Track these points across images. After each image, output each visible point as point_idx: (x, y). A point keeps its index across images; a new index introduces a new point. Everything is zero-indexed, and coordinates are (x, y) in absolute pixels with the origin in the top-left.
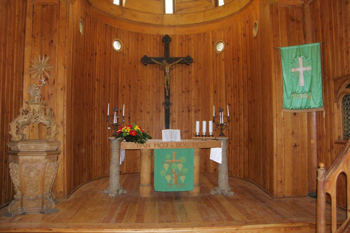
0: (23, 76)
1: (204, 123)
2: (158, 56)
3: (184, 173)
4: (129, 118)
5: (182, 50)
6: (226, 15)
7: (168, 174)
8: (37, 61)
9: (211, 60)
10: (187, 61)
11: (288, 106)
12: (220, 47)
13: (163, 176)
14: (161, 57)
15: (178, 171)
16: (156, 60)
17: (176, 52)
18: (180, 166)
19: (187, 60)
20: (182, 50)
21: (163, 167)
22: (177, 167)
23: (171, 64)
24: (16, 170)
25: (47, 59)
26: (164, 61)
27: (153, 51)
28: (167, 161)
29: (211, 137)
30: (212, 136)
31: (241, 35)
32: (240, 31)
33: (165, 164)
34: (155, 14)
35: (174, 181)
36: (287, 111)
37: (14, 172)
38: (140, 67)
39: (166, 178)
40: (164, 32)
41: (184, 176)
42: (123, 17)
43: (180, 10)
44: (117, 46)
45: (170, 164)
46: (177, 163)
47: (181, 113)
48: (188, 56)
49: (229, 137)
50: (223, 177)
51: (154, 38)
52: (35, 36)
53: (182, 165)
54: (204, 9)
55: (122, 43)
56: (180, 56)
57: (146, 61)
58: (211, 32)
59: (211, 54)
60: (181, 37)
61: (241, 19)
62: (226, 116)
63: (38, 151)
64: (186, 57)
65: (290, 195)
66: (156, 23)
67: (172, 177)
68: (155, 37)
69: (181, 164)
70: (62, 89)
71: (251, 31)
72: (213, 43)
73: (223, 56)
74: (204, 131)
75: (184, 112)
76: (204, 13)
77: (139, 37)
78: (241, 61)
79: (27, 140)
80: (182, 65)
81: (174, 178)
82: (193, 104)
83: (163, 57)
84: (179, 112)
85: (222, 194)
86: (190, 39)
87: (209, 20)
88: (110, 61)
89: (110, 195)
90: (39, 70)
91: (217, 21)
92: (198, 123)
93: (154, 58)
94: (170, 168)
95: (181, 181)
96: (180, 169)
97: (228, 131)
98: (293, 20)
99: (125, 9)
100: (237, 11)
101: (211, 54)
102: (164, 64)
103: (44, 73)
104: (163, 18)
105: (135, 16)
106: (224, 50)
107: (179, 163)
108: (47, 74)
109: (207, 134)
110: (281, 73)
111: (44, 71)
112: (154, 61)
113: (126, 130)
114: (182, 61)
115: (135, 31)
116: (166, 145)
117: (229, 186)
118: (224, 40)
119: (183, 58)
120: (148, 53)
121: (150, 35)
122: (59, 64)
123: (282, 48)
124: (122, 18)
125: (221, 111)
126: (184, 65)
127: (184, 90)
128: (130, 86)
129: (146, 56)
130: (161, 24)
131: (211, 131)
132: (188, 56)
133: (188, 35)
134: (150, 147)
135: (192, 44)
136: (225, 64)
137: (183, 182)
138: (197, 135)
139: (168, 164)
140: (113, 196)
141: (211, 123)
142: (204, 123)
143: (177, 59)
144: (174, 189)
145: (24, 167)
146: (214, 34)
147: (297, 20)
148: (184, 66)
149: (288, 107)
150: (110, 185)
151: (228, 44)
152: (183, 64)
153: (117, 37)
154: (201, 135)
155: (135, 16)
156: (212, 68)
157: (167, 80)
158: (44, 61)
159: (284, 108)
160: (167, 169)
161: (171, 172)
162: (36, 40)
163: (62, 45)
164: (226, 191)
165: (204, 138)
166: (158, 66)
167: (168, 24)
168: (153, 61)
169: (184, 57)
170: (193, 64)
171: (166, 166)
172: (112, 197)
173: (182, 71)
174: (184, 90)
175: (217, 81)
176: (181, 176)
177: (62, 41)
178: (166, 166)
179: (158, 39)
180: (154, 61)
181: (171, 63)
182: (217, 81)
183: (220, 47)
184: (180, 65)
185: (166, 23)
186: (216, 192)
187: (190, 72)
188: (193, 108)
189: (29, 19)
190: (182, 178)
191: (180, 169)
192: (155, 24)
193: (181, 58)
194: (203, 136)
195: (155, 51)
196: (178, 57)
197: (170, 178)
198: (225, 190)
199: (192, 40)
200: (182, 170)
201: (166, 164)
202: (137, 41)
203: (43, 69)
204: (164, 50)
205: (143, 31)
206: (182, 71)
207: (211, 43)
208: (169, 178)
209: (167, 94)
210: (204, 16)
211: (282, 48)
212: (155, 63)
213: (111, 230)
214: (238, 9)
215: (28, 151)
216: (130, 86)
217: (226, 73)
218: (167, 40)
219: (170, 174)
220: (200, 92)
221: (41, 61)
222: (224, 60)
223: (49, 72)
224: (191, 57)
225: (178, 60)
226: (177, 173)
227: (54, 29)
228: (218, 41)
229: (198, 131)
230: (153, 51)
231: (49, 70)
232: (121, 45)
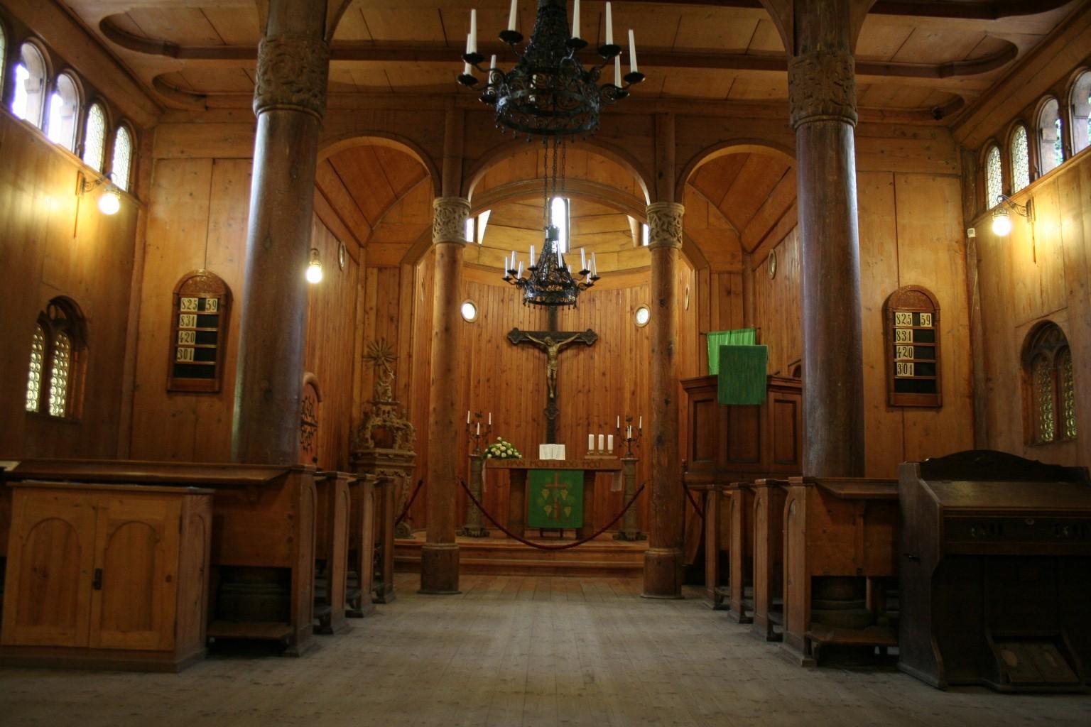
0: (972, 372)
1: (601, 437)
2: (537, 329)
14: (542, 330)
16: (534, 337)
18: (564, 494)
19: (587, 336)
28: (546, 486)
35: (555, 515)
39: (545, 508)
45: (551, 490)
48: (590, 330)
54: (618, 249)
55: (477, 309)
56: (577, 331)
64: (586, 331)
67: (553, 508)
72: (632, 309)
74: (601, 447)
76: (618, 256)
83: (546, 330)
86: (594, 300)
93: (532, 333)
94: (551, 496)
102: (547, 343)
113: (540, 60)
116: (545, 464)
119: (581, 333)
120: (521, 323)
124: (477, 263)
129: (516, 329)
131: (610, 447)
132: (590, 330)
134: (524, 465)
135: (597, 308)
142: (601, 437)
143: (569, 335)
153: (469, 298)
169: (583, 331)
171: (545, 493)
180: (530, 338)
181: (559, 342)
188: (596, 419)
190: (567, 511)
191: (564, 497)
193: (575, 333)
196: (572, 331)
202: (501, 304)
204: (198, 617)
207: (628, 308)
209: (552, 395)
210: (618, 260)
224: (593, 330)
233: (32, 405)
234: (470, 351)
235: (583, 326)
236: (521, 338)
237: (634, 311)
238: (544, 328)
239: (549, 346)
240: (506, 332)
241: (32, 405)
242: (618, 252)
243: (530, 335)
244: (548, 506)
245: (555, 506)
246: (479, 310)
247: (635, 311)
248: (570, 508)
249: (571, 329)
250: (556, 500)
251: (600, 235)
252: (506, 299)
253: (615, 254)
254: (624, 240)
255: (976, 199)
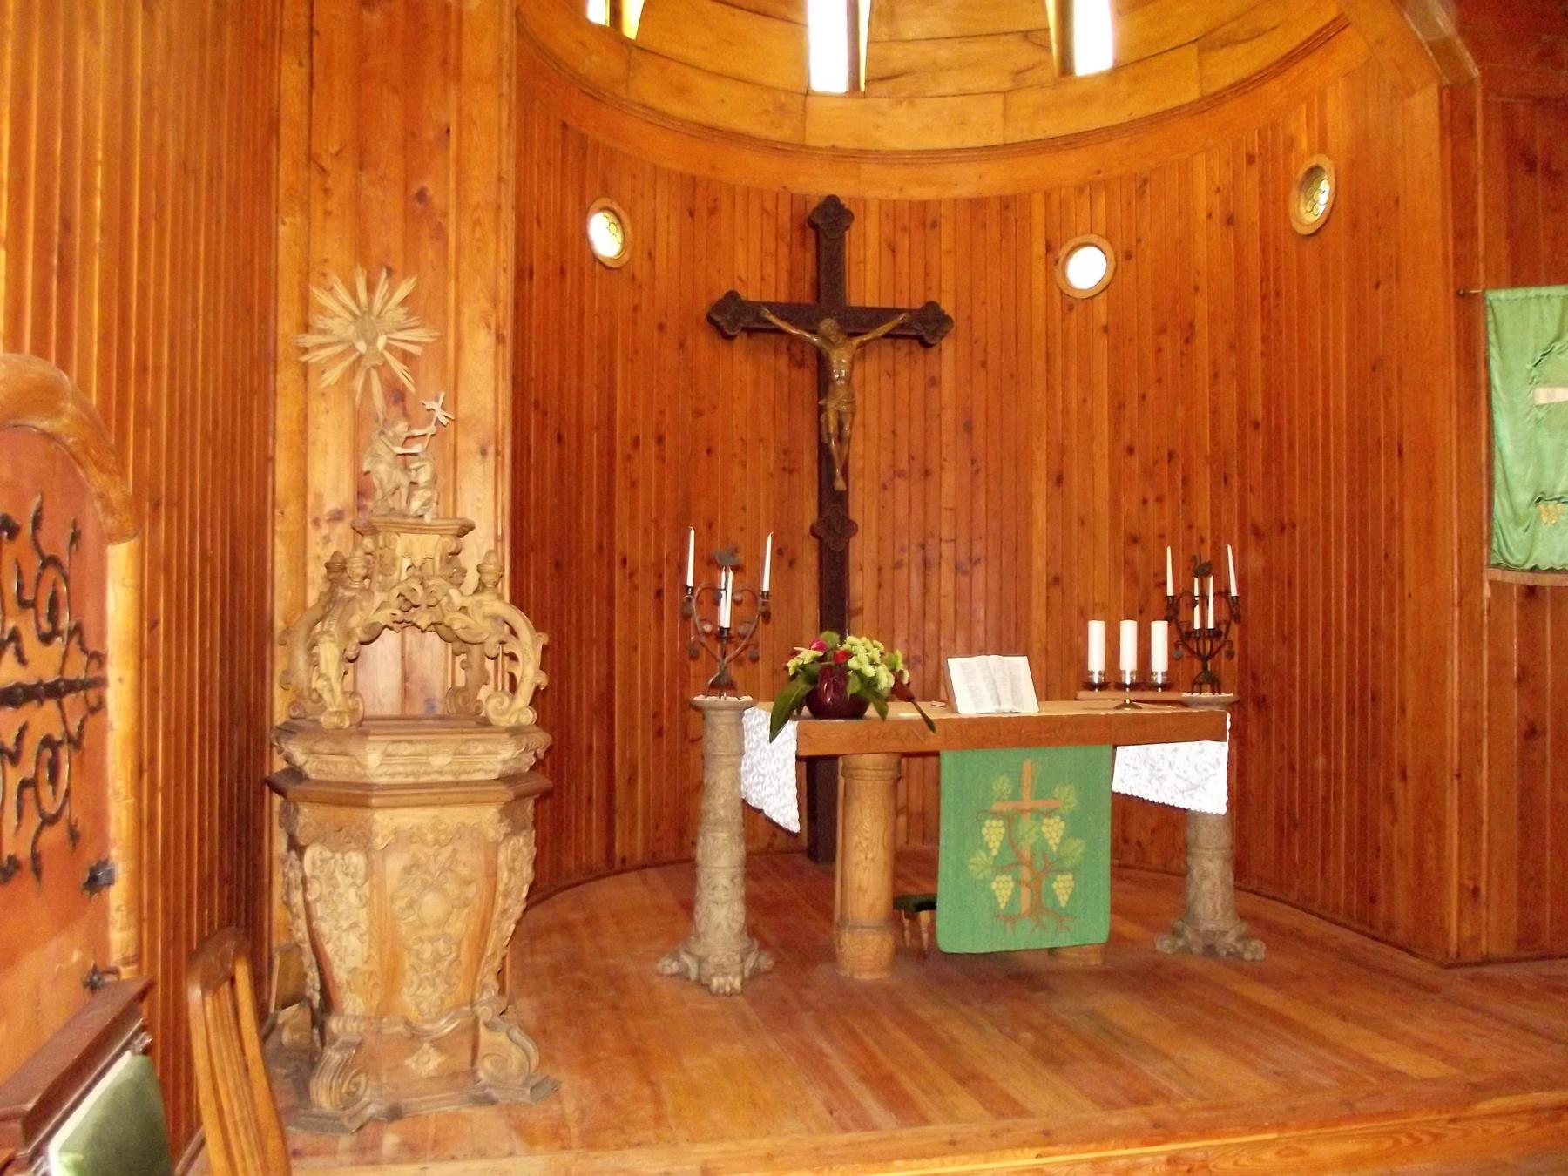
1: (1128, 629)
2: (783, 299)
3: (1068, 864)
4: (659, 594)
5: (895, 274)
6: (1120, 116)
7: (1000, 868)
8: (345, 298)
9: (1039, 328)
10: (923, 328)
11: (1517, 558)
12: (1087, 269)
13: (981, 877)
15: (1044, 854)
16: (783, 319)
17: (867, 285)
18: (1053, 831)
20: (895, 274)
21: (982, 837)
22: (1039, 833)
23: (857, 341)
24: (354, 884)
25: (404, 290)
26: (827, 325)
27: (759, 269)
28: (996, 807)
29: (1160, 694)
30: (1165, 687)
31: (1210, 216)
32: (1203, 200)
33: (988, 823)
34: (770, 89)
36: (1510, 577)
37: (341, 895)
38: (704, 344)
39: (994, 886)
40: (820, 183)
41: (1070, 877)
42: (627, 90)
43: (889, 78)
44: (605, 237)
45: (1010, 821)
46: (1040, 815)
47: (887, 575)
49: (1239, 692)
50: (1210, 873)
51: (764, 210)
52: (327, 163)
53: (1062, 825)
54: (1007, 85)
55: (629, 229)
57: (732, 318)
58: (1038, 198)
59: (1039, 299)
60: (892, 212)
61: (1210, 142)
62: (1222, 593)
63: (464, 777)
65: (1508, 949)
66: (776, 135)
67: (1018, 882)
68: (770, 206)
69: (1058, 818)
70: (484, 452)
71: (1275, 204)
72: (1049, 248)
73: (1101, 311)
75: (905, 570)
76: (1005, 103)
77: (700, 200)
78: (1202, 340)
79: (416, 718)
80: (893, 344)
81: (1028, 885)
82: (946, 533)
84: (880, 569)
85: (1229, 953)
86: (935, 225)
87: (1030, 138)
88: (582, 311)
89: (716, 982)
90: (361, 347)
91: (1071, 142)
92: (1096, 630)
93: (776, 308)
94: (1011, 842)
95: (1055, 898)
96: (1051, 842)
97: (29, 597)
98: (1531, 166)
99: (635, 53)
100: (1187, 100)
101: (1039, 299)
103: (386, 363)
104: (804, 113)
105: (681, 90)
106: (1108, 287)
107: (1049, 815)
108: (398, 367)
109: (1144, 679)
110: (1483, 402)
111: (388, 356)
112: (773, 319)
114: (902, 326)
115: (679, 168)
117: (739, 871)
118: (1107, 237)
119: (910, 311)
121: (748, 191)
122: (465, 320)
123: (1492, 295)
125: (1202, 573)
126: (904, 346)
127: (904, 465)
128: (660, 440)
129: (732, 296)
130: (796, 141)
131: (1159, 663)
132: (932, 306)
133: (924, 205)
135: (944, 246)
136: (1114, 348)
137: (1063, 904)
138: (1096, 681)
139: (1001, 823)
140: (732, 988)
141: (1160, 630)
142: (1128, 629)
144: (1022, 938)
145: (395, 865)
146: (1055, 204)
147: (1547, 166)
148: (905, 349)
149: (1512, 561)
150: (704, 934)
151: (1128, 256)
152: (901, 341)
153: (606, 191)
154: (1112, 682)
155: (681, 90)
156: (1040, 366)
157: (839, 413)
158: (392, 298)
159: (1497, 566)
160: (998, 845)
161: (1012, 859)
162: (330, 184)
163: (477, 222)
164: (1231, 938)
165: (1128, 696)
166: (784, 344)
167: (828, 144)
168: (769, 322)
170: (947, 347)
171: (994, 832)
172: (728, 989)
173: (893, 375)
174: (904, 465)
175: (1066, 428)
176: (1059, 878)
177: (475, 199)
178: (994, 832)
179: (785, 214)
180: (773, 319)
182: (1066, 428)
183: (1087, 269)
184: (887, 348)
185: (818, 136)
186: (1181, 943)
187: (934, 382)
189: (295, 66)
190: (1062, 887)
191: (1054, 843)
192: (766, 140)
194: (1121, 686)
195: (770, 270)
197: (1012, 885)
198: (1224, 933)
199: (946, 228)
200: (1061, 845)
201: (994, 823)
203: (381, 342)
205: (713, 168)
206: (893, 375)
208: (1003, 888)
211: (1492, 295)
212: (779, 331)
213: (926, 1162)
214: (1193, 94)
215: (411, 780)
216: (660, 440)
217: (1115, 393)
218: (826, 225)
219: (1010, 866)
220: (982, 475)
221: (370, 302)
222: (1106, 329)
223: (406, 358)
225: (887, 320)
226: (1039, 864)
227: (430, 134)
228: (1078, 240)
229: (1096, 663)
230: (759, 269)
231: (409, 347)
232: (624, 234)
233: (1197, 626)
234: (612, 350)
235: (906, 296)
236: (748, 320)
237: (1055, 254)
238: (805, 295)
239: (833, 345)
240: (703, 307)
241: (1197, 626)
242: (1006, 92)
243: (774, 313)
244: (1004, 878)
245: (1025, 874)
246: (634, 222)
247: (1062, 254)
248: (1070, 877)
249: (871, 302)
250: (1026, 854)
251: (954, 44)
252: (702, 207)
253: (1000, 98)
254: (1025, 55)
255: (497, 290)
